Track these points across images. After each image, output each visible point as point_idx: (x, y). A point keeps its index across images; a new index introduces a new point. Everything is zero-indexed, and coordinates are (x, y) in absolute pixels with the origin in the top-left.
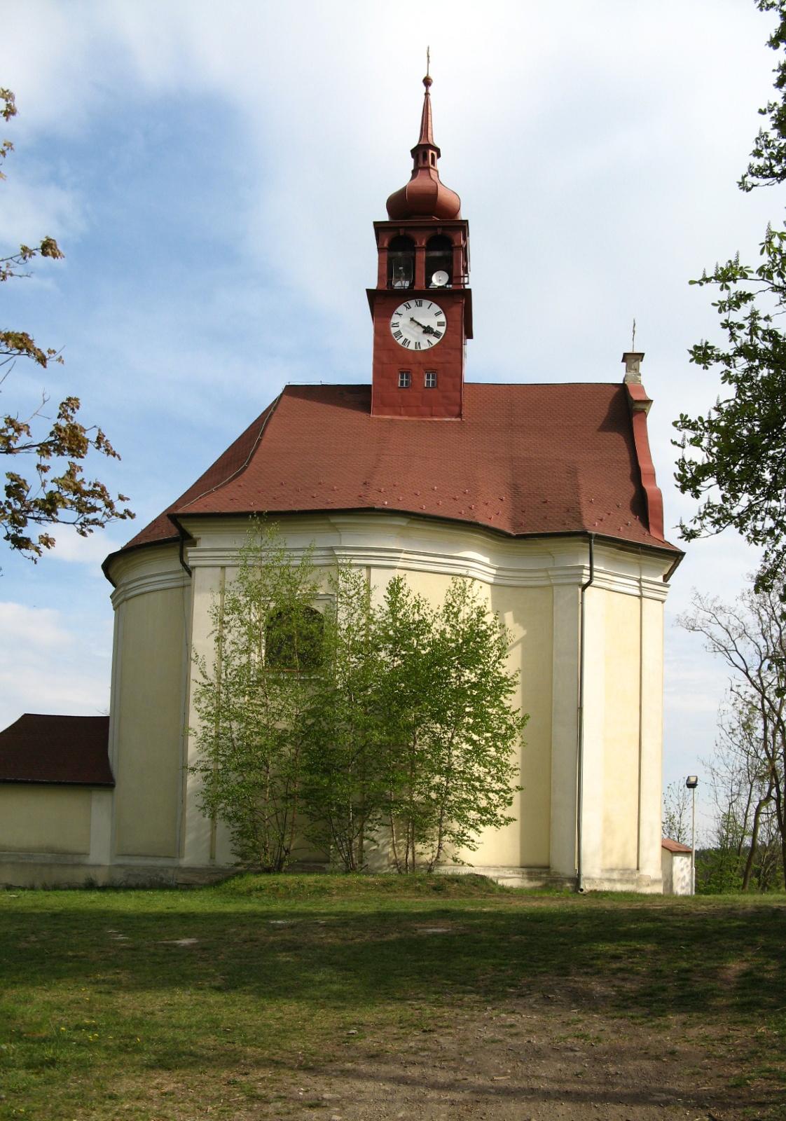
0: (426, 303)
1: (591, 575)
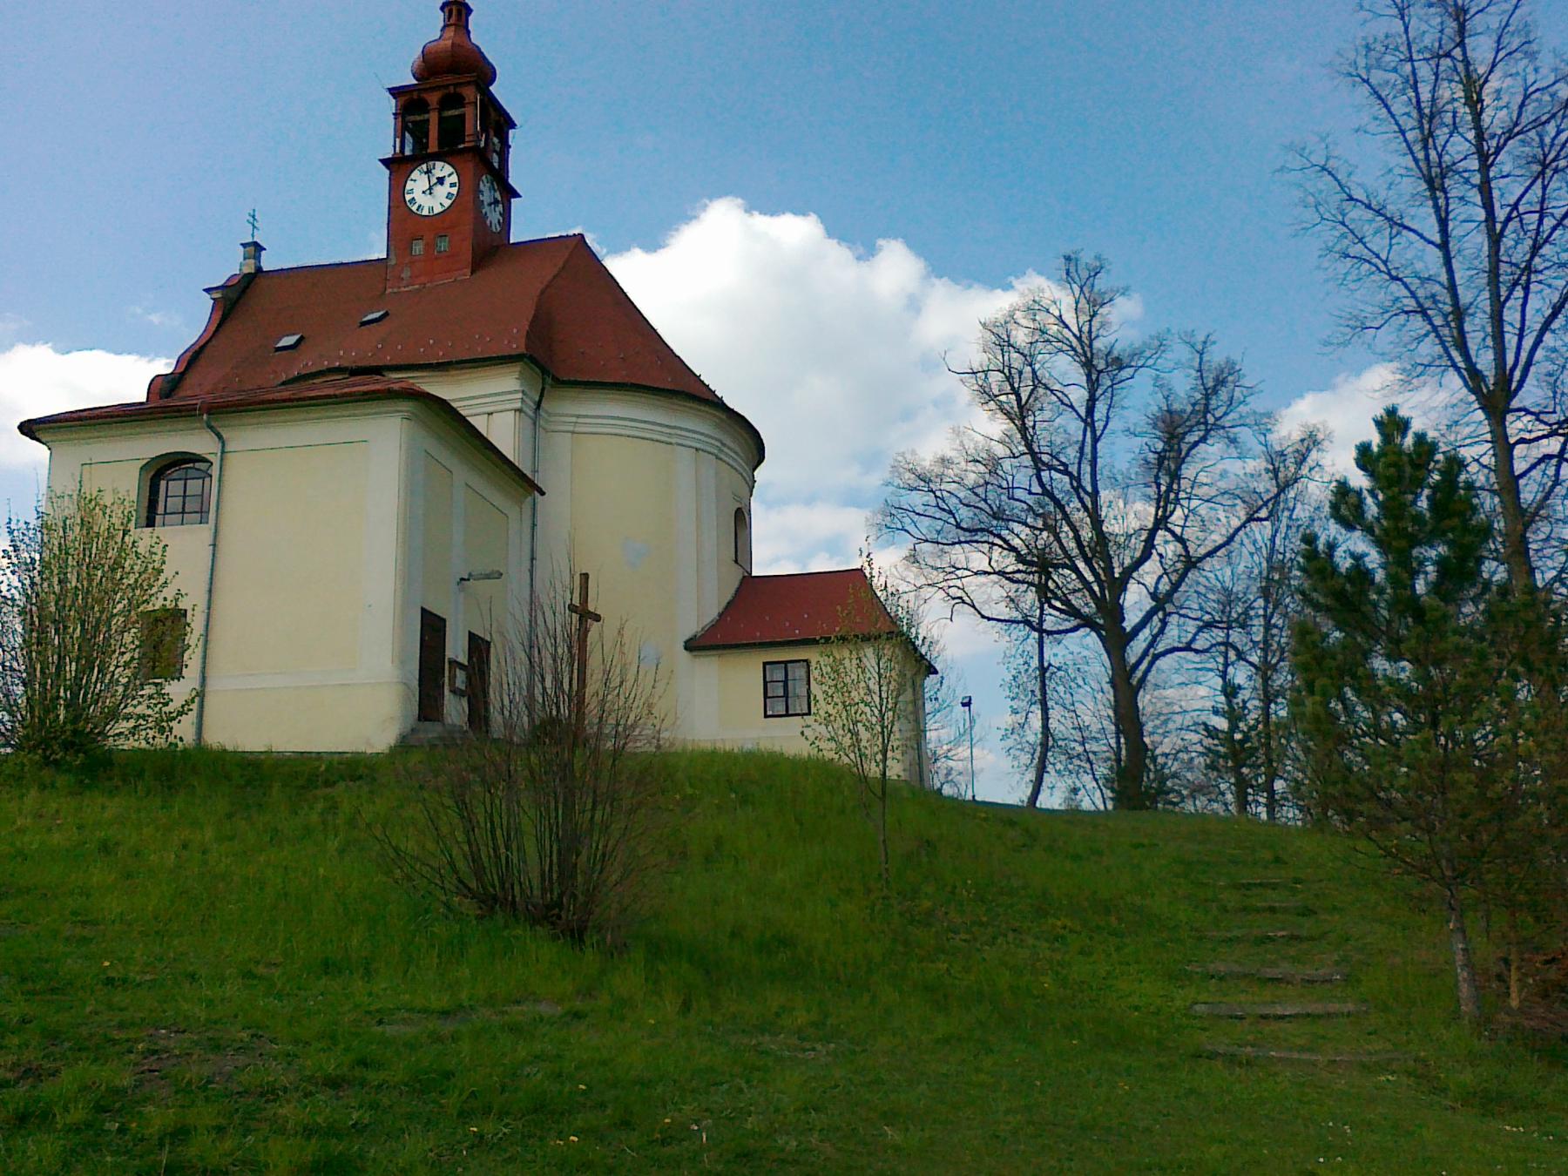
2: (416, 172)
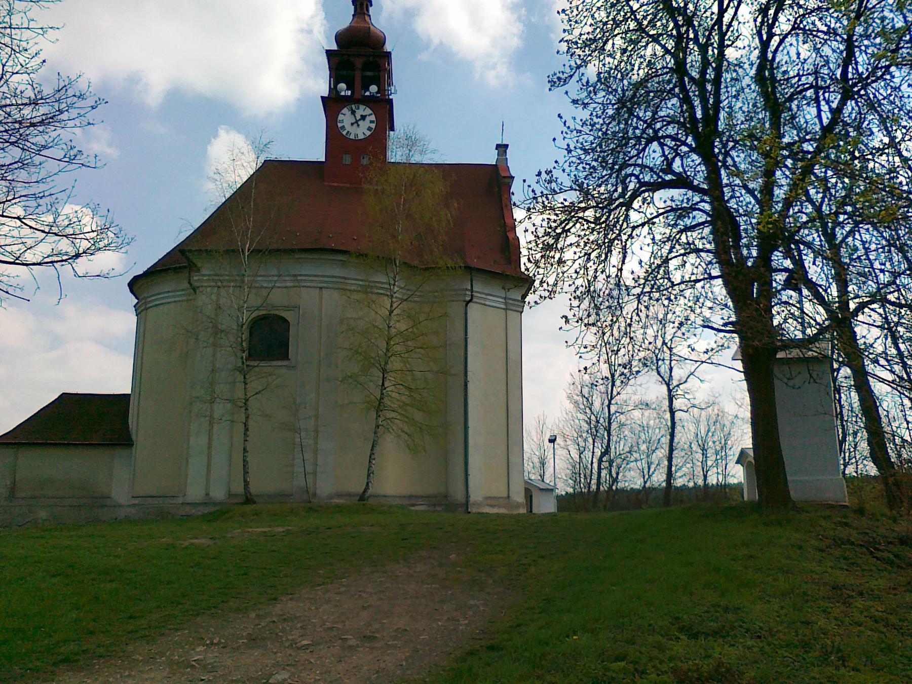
2: (345, 109)
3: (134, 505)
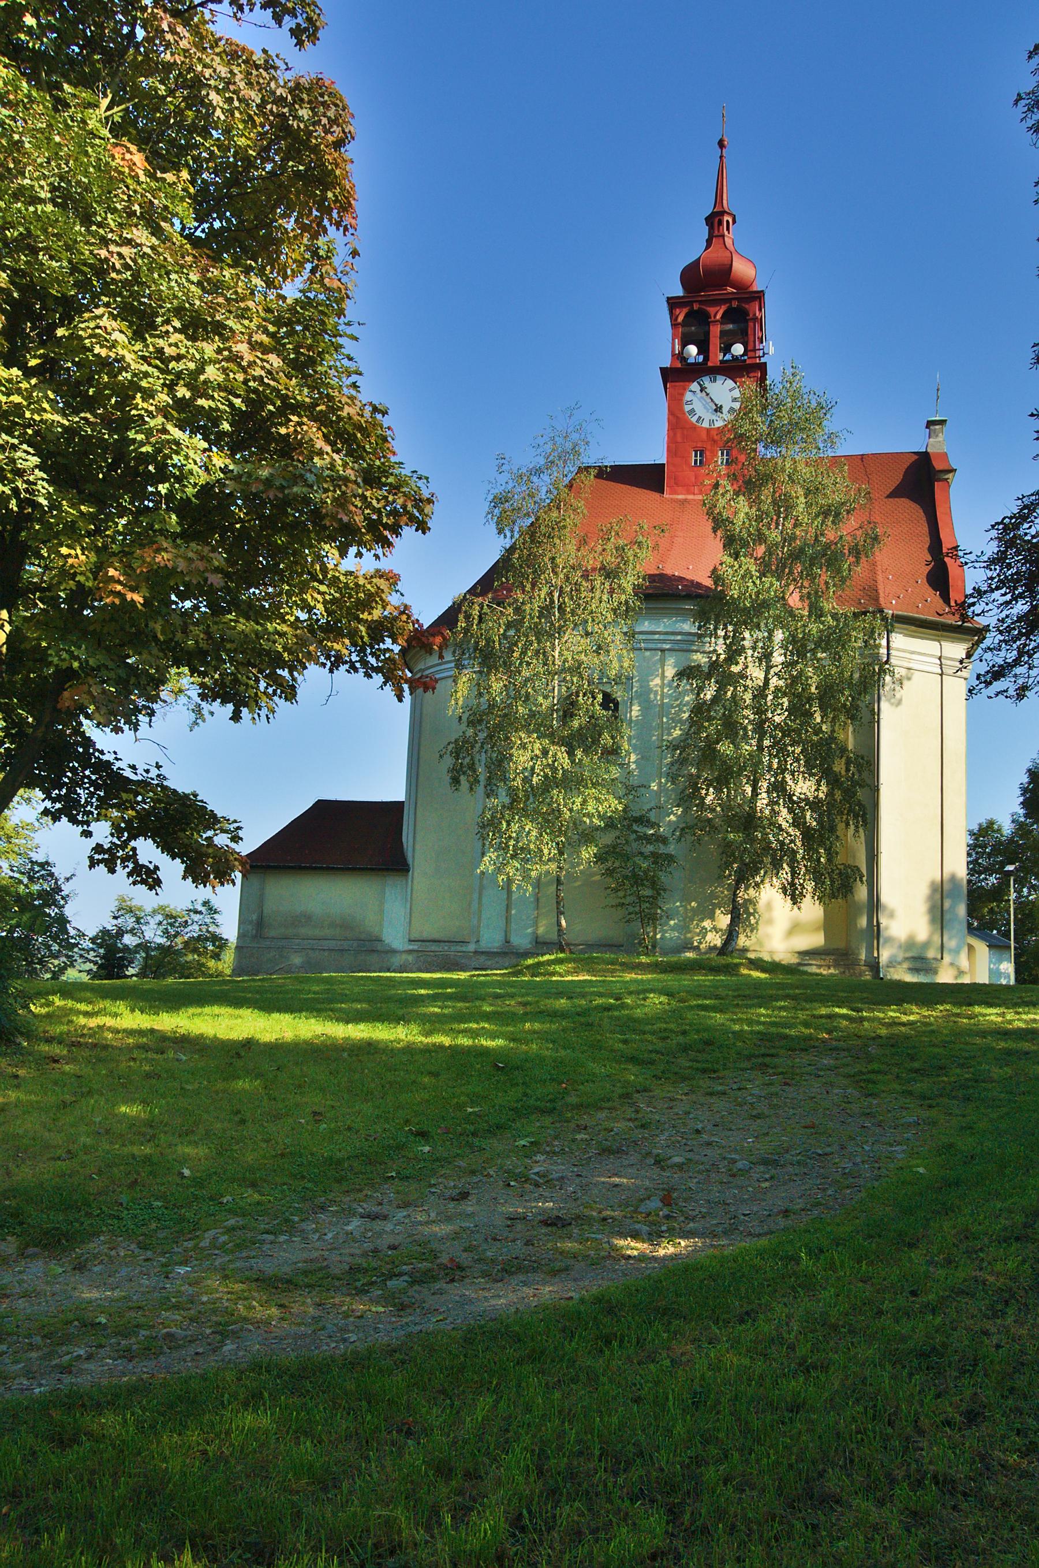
0: (720, 379)
1: (888, 654)
3: (410, 952)
